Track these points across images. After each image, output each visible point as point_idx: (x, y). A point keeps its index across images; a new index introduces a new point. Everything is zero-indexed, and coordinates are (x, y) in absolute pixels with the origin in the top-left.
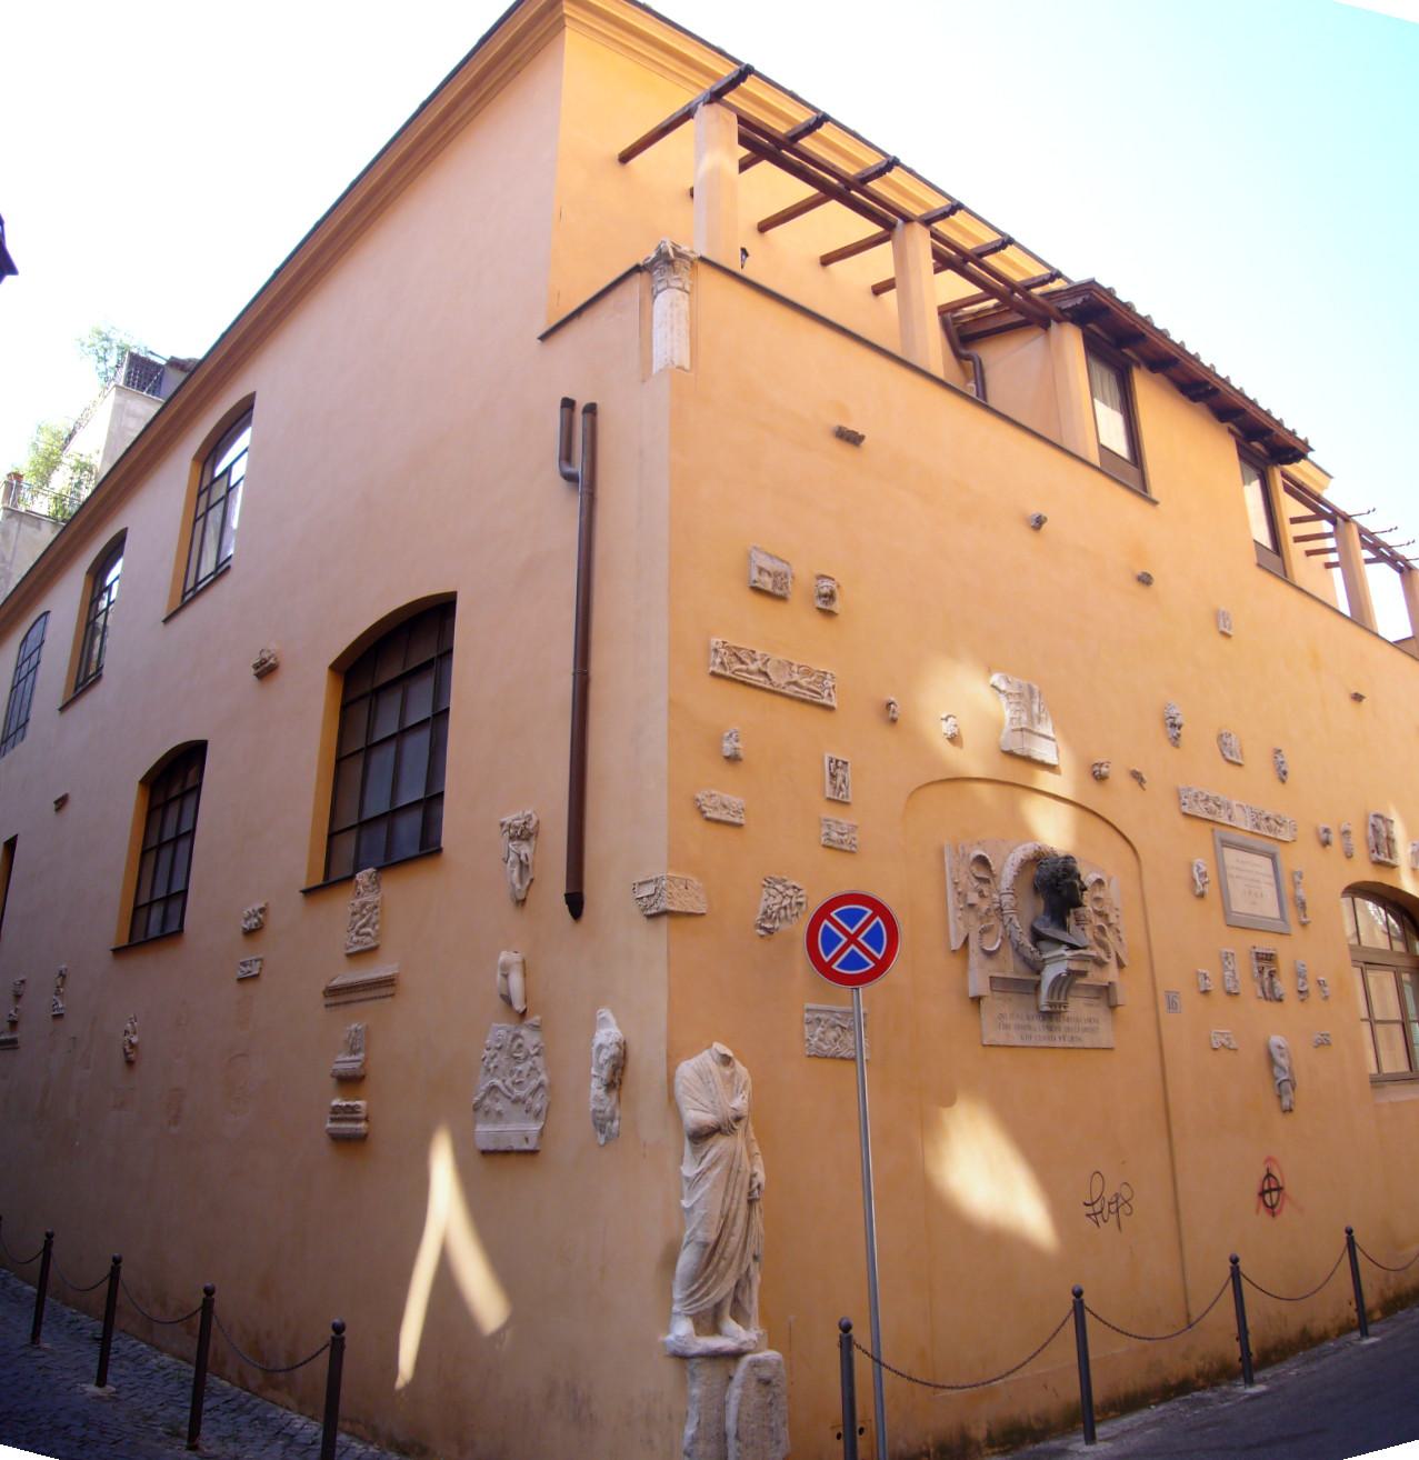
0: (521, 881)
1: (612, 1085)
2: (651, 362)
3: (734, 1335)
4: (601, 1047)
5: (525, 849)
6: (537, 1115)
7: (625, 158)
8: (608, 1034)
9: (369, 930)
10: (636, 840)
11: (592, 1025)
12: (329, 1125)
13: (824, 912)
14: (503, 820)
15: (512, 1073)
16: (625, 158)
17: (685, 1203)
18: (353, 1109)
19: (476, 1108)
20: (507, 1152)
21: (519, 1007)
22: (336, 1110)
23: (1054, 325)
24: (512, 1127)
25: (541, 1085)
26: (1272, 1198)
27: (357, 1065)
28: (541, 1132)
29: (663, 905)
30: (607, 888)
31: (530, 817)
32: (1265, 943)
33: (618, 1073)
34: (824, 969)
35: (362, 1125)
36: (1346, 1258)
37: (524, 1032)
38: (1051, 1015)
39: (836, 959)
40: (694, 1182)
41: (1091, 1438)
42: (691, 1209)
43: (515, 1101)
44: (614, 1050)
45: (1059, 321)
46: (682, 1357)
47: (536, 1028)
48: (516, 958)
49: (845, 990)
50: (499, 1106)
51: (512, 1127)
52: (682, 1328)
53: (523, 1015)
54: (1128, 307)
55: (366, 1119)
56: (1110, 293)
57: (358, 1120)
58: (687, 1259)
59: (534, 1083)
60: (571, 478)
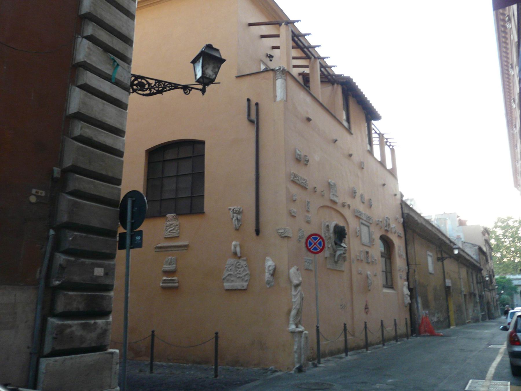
0: (238, 224)
1: (273, 275)
2: (276, 96)
3: (301, 328)
4: (270, 266)
5: (239, 217)
6: (246, 281)
7: (250, 25)
8: (270, 263)
9: (174, 231)
10: (275, 217)
11: (264, 261)
12: (161, 284)
13: (309, 237)
14: (230, 208)
15: (237, 271)
16: (250, 25)
17: (293, 300)
18: (173, 280)
19: (223, 279)
20: (235, 290)
21: (239, 255)
22: (165, 280)
23: (336, 85)
24: (237, 284)
25: (247, 274)
26: (367, 310)
27: (174, 268)
28: (248, 285)
29: (286, 235)
30: (267, 229)
31: (240, 208)
32: (367, 249)
33: (274, 273)
34: (309, 250)
35: (177, 284)
36: (344, 333)
37: (240, 261)
38: (336, 262)
39: (311, 248)
40: (295, 296)
41: (347, 355)
42: (295, 302)
43: (239, 277)
44: (274, 267)
45: (337, 84)
46: (293, 333)
47: (244, 260)
48: (238, 243)
49: (313, 255)
50: (232, 279)
51: (237, 284)
52: (292, 327)
53: (240, 257)
54: (355, 83)
55: (178, 283)
56: (352, 79)
57: (175, 283)
58: (293, 312)
59: (245, 274)
60: (252, 121)
